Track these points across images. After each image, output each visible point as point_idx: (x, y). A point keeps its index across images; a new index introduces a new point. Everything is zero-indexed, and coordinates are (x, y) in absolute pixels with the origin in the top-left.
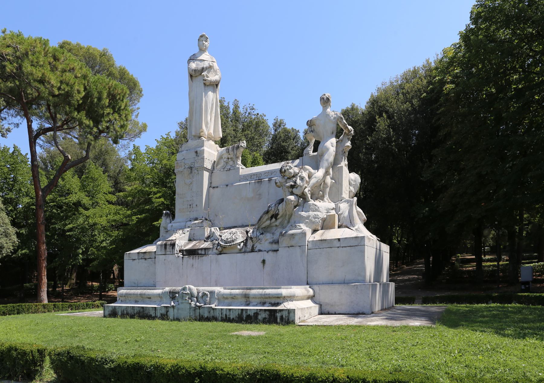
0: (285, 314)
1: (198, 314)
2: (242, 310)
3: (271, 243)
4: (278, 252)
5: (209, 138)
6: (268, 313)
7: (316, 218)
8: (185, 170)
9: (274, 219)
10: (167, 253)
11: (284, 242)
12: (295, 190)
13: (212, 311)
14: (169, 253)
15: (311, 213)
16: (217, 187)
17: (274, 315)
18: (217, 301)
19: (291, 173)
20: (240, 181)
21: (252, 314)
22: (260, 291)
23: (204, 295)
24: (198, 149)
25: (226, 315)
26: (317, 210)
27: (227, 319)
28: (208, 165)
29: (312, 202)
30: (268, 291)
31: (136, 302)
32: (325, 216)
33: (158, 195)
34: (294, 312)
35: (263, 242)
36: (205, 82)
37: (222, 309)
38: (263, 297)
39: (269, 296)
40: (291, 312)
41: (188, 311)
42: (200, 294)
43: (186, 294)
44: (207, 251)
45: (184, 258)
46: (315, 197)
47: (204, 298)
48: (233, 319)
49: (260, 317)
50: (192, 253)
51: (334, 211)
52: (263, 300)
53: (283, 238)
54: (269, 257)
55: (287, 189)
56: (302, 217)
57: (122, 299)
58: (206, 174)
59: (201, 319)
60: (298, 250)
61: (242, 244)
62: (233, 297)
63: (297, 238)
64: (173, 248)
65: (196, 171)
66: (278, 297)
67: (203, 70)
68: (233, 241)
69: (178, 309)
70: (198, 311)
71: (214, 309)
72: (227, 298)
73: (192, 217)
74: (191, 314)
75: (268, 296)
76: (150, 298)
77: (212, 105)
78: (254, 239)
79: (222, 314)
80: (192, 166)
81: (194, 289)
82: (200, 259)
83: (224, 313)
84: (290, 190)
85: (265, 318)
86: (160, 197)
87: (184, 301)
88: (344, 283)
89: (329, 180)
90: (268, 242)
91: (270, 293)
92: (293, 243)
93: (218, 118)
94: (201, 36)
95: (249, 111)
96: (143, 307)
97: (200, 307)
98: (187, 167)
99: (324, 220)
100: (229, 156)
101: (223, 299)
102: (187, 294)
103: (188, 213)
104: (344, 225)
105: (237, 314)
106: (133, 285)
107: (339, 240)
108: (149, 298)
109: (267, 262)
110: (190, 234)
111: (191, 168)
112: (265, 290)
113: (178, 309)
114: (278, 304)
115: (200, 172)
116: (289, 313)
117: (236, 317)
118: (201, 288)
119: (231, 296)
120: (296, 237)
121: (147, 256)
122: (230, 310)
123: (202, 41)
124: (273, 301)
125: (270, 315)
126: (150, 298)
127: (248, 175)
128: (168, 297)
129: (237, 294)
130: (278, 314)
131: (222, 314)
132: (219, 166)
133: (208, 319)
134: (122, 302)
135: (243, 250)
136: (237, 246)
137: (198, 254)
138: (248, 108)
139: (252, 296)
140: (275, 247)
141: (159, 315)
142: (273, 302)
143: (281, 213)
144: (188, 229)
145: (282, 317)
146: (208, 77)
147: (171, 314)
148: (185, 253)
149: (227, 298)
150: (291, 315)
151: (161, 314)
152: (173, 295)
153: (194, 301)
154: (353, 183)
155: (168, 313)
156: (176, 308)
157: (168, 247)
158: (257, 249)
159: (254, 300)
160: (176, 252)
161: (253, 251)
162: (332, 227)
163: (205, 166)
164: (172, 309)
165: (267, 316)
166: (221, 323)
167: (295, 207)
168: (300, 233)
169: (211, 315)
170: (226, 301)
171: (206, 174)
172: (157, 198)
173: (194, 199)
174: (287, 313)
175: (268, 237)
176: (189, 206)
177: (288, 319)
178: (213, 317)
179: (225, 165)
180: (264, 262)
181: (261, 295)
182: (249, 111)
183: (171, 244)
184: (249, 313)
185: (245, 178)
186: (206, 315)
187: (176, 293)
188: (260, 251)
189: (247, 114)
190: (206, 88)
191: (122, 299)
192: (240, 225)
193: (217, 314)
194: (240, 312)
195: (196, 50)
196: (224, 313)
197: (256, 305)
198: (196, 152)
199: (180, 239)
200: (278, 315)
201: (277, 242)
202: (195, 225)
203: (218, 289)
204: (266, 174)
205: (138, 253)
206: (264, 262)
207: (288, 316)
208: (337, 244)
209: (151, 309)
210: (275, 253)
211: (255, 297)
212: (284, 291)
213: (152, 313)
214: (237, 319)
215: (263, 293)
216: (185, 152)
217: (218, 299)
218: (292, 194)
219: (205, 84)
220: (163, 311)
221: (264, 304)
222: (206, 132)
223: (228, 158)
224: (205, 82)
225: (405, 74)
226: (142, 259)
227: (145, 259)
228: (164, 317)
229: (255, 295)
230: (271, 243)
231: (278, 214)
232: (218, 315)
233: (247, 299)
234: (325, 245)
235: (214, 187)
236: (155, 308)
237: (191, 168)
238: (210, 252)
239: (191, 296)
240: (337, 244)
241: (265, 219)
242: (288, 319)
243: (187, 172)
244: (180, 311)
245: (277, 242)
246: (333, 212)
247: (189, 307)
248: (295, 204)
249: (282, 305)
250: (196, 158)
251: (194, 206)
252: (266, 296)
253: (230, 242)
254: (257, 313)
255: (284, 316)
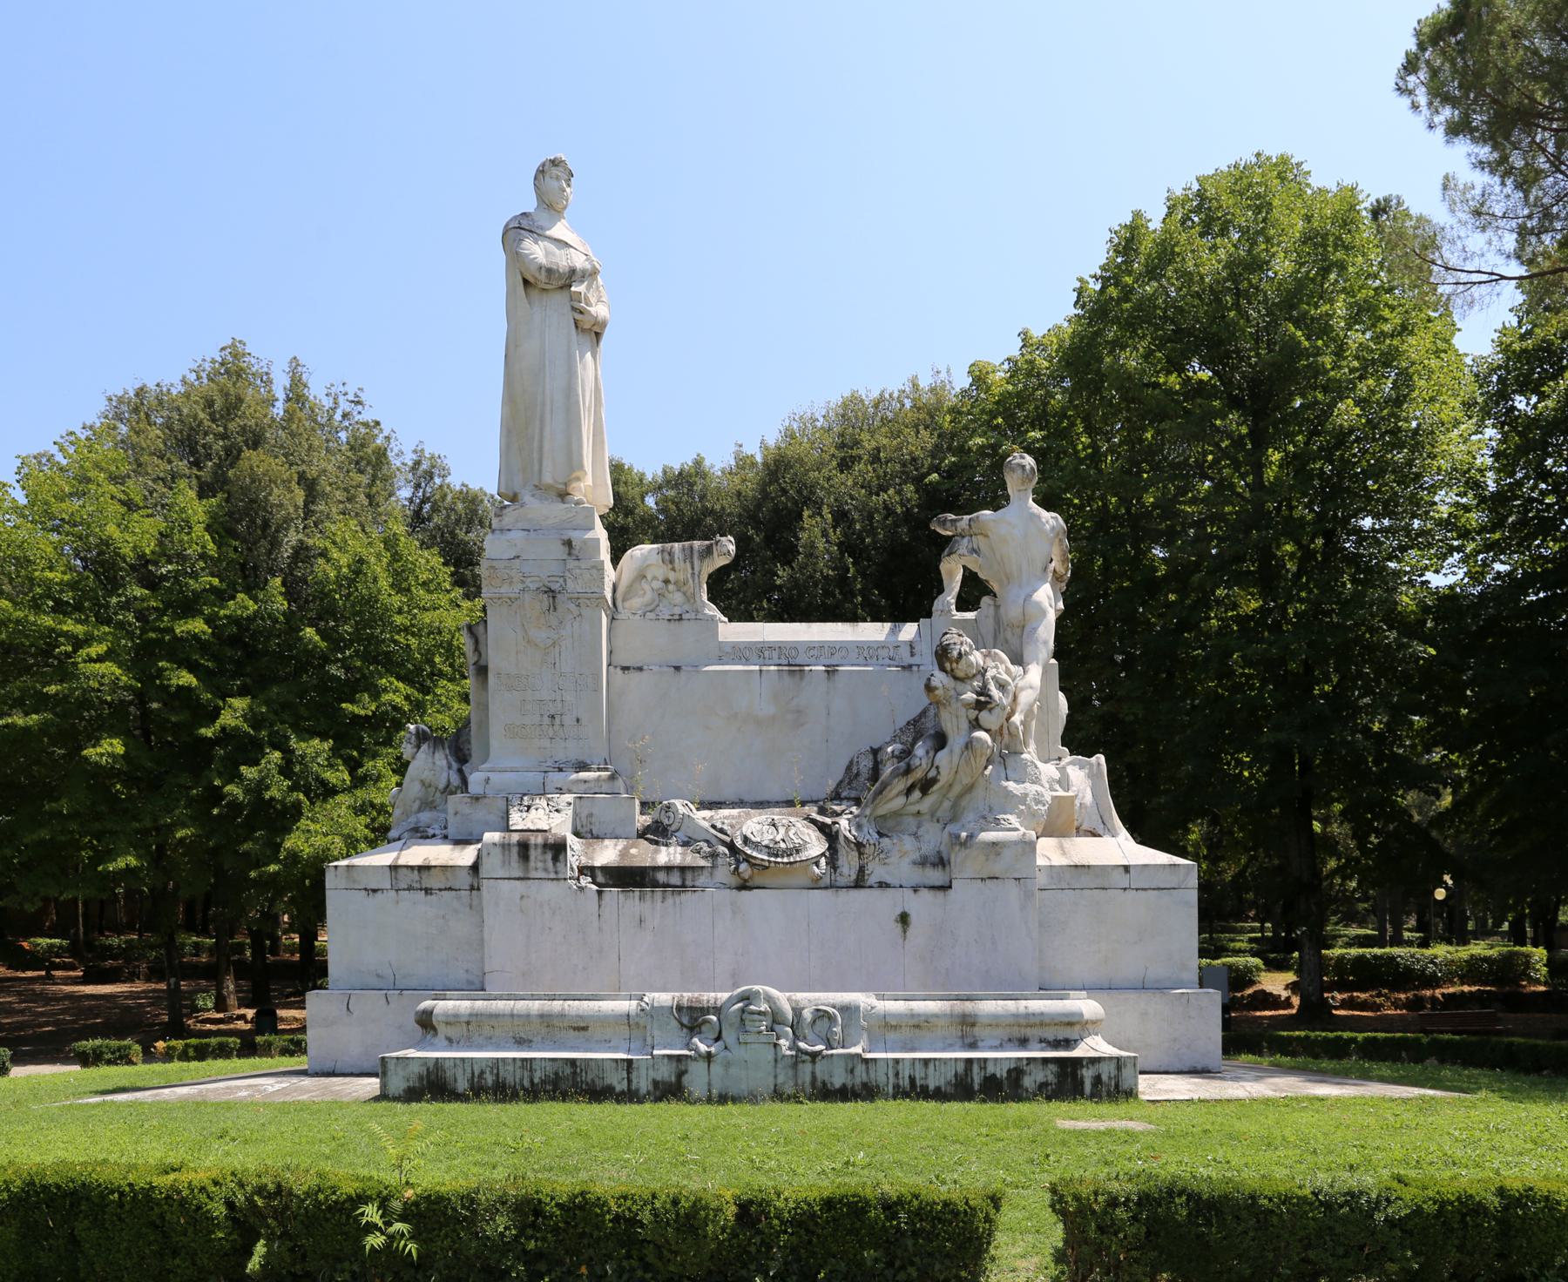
0: (1106, 1071)
1: (808, 1079)
2: (969, 1061)
3: (923, 862)
4: (951, 892)
6: (1053, 1067)
8: (527, 597)
9: (917, 794)
10: (533, 874)
11: (965, 865)
12: (984, 717)
13: (860, 1069)
14: (541, 874)
16: (640, 669)
17: (1074, 1075)
18: (865, 1035)
19: (970, 665)
20: (720, 661)
21: (1001, 1072)
22: (1011, 1006)
23: (820, 1015)
24: (574, 535)
25: (912, 1080)
26: (1036, 781)
27: (915, 1090)
30: (1036, 1006)
31: (521, 1043)
33: (97, 649)
35: (893, 860)
36: (578, 317)
37: (897, 1061)
38: (1022, 1021)
39: (1041, 1020)
41: (770, 1067)
42: (807, 1014)
44: (689, 876)
45: (606, 897)
48: (938, 1089)
49: (1028, 1082)
50: (627, 878)
52: (1017, 1032)
53: (963, 853)
54: (922, 906)
55: (963, 712)
56: (1008, 794)
57: (452, 1032)
59: (826, 1093)
60: (1012, 891)
61: (823, 861)
62: (919, 1024)
63: (1007, 854)
64: (555, 859)
65: (572, 607)
66: (1070, 1024)
68: (798, 851)
69: (727, 1065)
70: (806, 1069)
71: (867, 1061)
72: (895, 1028)
73: (561, 756)
74: (781, 1079)
75: (1037, 1020)
76: (585, 1029)
78: (868, 850)
79: (897, 1074)
80: (555, 587)
81: (784, 999)
82: (670, 901)
83: (905, 1073)
84: (973, 714)
85: (1043, 1086)
86: (100, 659)
88: (1142, 987)
90: (907, 860)
91: (1043, 1009)
92: (997, 868)
94: (555, 163)
95: (344, 406)
96: (573, 1062)
97: (814, 1056)
98: (533, 586)
100: (672, 576)
101: (886, 1027)
103: (546, 743)
104: (1085, 827)
105: (950, 1075)
106: (375, 982)
107: (1126, 868)
108: (580, 1028)
109: (913, 919)
110: (576, 814)
111: (551, 593)
112: (1023, 1003)
113: (727, 1065)
114: (1068, 1044)
115: (585, 612)
116: (1119, 1068)
117: (949, 1083)
118: (801, 996)
119: (912, 1022)
120: (1007, 853)
121: (432, 881)
122: (926, 1062)
123: (558, 178)
124: (1050, 1034)
125: (1061, 1076)
126: (585, 1029)
127: (749, 646)
128: (675, 1023)
129: (936, 1016)
130: (1084, 1071)
131: (897, 1074)
132: (636, 602)
133: (845, 1094)
134: (451, 1043)
135: (827, 881)
136: (806, 868)
137: (655, 884)
138: (341, 399)
139: (987, 1021)
140: (936, 876)
141: (643, 1085)
142: (1051, 1038)
143: (944, 778)
144: (569, 797)
145: (1097, 1079)
147: (697, 1079)
148: (600, 879)
149: (895, 1028)
151: (656, 1083)
152: (692, 1019)
155: (686, 1079)
156: (718, 1059)
157: (533, 853)
158: (872, 880)
159: (988, 1031)
160: (569, 874)
161: (859, 883)
164: (703, 1065)
165: (1051, 1078)
166: (892, 1105)
168: (1015, 843)
169: (858, 1081)
170: (891, 1036)
172: (91, 660)
173: (568, 697)
174: (1113, 1066)
176: (547, 720)
177: (1117, 1086)
178: (865, 1085)
180: (904, 919)
181: (1016, 1016)
182: (344, 406)
183: (546, 846)
184: (991, 1069)
185: (740, 652)
186: (838, 1081)
187: (705, 1011)
188: (883, 885)
189: (338, 417)
191: (452, 1032)
192: (734, 798)
193: (880, 1077)
194: (961, 1068)
195: (530, 204)
196: (905, 1073)
197: (1000, 1047)
198: (568, 543)
200: (1087, 1074)
201: (941, 862)
202: (583, 787)
203: (863, 999)
204: (814, 652)
205: (394, 868)
206: (904, 919)
207: (1117, 1077)
208: (1124, 881)
209: (607, 1066)
210: (940, 894)
211: (995, 1021)
213: (617, 1081)
214: (950, 1090)
215: (1022, 1010)
216: (517, 535)
217: (868, 1030)
220: (666, 1073)
221: (1023, 1043)
223: (667, 582)
224: (578, 317)
225: (850, 410)
226: (410, 889)
227: (428, 891)
228: (671, 1090)
229: (996, 1016)
230: (923, 862)
231: (934, 781)
232: (882, 1079)
233: (967, 1029)
234: (1086, 881)
235: (625, 669)
236: (630, 1062)
237: (551, 593)
238: (702, 880)
239: (776, 1018)
240: (1124, 881)
241: (895, 792)
242: (1117, 1086)
243: (535, 605)
244: (733, 1071)
245: (941, 862)
247: (771, 1057)
249: (1082, 1045)
250: (571, 564)
251: (569, 720)
252: (1032, 1020)
253: (788, 852)
254: (1017, 1071)
255: (1104, 1078)
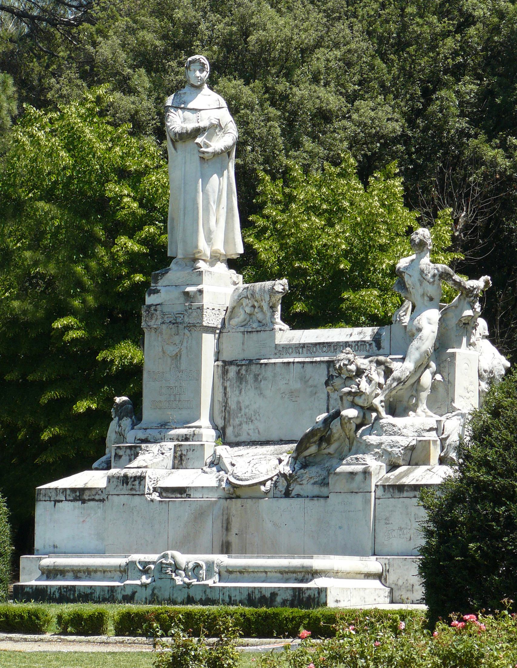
4: (329, 499)
5: (215, 259)
7: (394, 446)
15: (385, 439)
18: (217, 576)
19: (350, 371)
21: (268, 595)
28: (212, 319)
29: (387, 419)
31: (77, 578)
32: (414, 443)
34: (326, 591)
36: (202, 155)
40: (322, 591)
43: (167, 564)
46: (393, 409)
47: (196, 571)
49: (279, 599)
51: (434, 433)
58: (209, 342)
67: (198, 132)
77: (220, 191)
87: (163, 576)
89: (426, 379)
93: (233, 215)
96: (91, 587)
99: (411, 449)
102: (170, 564)
132: (234, 322)
146: (207, 146)
150: (323, 595)
153: (180, 575)
154: (485, 375)
158: (293, 493)
162: (426, 462)
163: (205, 324)
167: (358, 427)
171: (209, 342)
175: (313, 472)
179: (245, 320)
188: (298, 496)
190: (206, 165)
193: (215, 596)
199: (156, 465)
212: (318, 562)
218: (353, 405)
219: (202, 159)
220: (128, 592)
222: (202, 244)
239: (176, 568)
246: (432, 436)
248: (358, 421)
